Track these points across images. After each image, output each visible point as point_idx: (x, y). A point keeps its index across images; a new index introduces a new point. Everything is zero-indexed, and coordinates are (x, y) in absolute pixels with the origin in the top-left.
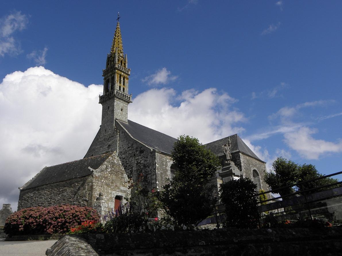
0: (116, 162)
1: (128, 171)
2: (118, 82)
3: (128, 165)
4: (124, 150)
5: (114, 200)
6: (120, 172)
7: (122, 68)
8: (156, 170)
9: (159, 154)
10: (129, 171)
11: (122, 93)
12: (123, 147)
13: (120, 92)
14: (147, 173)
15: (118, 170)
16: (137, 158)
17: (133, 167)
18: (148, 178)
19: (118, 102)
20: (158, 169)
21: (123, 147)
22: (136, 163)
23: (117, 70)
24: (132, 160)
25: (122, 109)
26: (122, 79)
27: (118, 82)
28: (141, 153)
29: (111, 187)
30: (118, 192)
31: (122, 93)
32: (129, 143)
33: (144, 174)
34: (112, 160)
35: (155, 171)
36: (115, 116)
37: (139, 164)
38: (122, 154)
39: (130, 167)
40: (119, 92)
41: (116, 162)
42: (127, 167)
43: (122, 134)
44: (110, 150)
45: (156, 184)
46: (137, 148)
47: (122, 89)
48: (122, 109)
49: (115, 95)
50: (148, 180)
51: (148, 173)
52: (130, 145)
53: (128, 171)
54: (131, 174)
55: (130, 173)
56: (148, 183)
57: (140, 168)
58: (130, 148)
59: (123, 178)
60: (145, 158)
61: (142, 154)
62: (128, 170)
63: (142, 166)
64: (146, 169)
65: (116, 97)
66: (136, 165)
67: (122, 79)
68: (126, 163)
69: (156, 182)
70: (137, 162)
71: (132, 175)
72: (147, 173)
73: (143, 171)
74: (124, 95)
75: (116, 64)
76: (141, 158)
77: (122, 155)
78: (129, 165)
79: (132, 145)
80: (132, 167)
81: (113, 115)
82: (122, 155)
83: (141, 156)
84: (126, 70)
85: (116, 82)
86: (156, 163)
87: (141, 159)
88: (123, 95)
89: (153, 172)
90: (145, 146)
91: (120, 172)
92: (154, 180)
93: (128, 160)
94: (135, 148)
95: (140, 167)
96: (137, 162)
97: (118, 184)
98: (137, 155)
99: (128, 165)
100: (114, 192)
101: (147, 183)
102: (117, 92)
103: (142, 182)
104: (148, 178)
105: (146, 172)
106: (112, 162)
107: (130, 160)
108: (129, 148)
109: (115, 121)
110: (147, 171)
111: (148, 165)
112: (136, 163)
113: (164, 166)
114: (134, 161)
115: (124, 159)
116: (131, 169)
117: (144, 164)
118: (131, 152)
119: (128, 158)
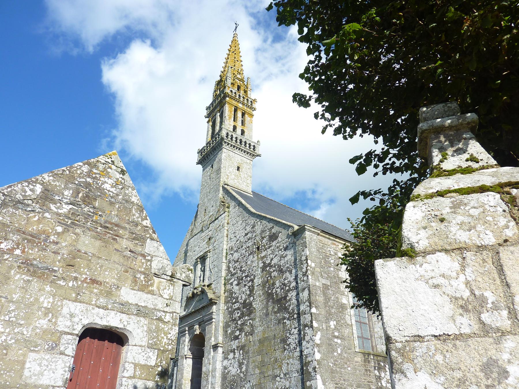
0: (113, 190)
1: (244, 289)
2: (230, 118)
3: (244, 275)
4: (238, 242)
5: (70, 346)
6: (125, 228)
7: (239, 95)
8: (308, 276)
9: (315, 237)
10: (247, 287)
11: (239, 138)
12: (235, 236)
13: (233, 134)
14: (287, 288)
15: (115, 220)
16: (262, 255)
17: (254, 278)
18: (289, 300)
19: (231, 154)
20: (313, 273)
21: (235, 236)
22: (261, 268)
23: (228, 97)
24: (252, 262)
25: (238, 168)
26: (239, 114)
27: (230, 118)
28: (273, 242)
29: (62, 283)
30: (105, 308)
31: (239, 138)
32: (247, 224)
33: (279, 290)
34: (89, 176)
35: (305, 278)
36: (223, 179)
37: (268, 269)
38: (232, 252)
39: (249, 279)
40: (232, 135)
41: (113, 190)
42: (242, 279)
43: (234, 210)
44: (211, 247)
45: (311, 314)
46: (263, 231)
47: (239, 131)
48: (238, 168)
49: (222, 139)
50: (290, 306)
51: (289, 286)
52: (249, 229)
53: (244, 289)
54: (250, 296)
55: (248, 293)
56: (289, 313)
57: (271, 277)
58: (249, 235)
59: (144, 256)
60: (281, 250)
61: (274, 243)
62: (245, 285)
63: (274, 271)
64: (284, 277)
65: (225, 142)
66: (262, 272)
67: (239, 114)
68: (241, 271)
69: (311, 308)
70: (264, 263)
71: (252, 298)
72: (287, 288)
73: (278, 284)
74: (244, 140)
75: (227, 87)
76: (273, 253)
77: (232, 254)
78: (246, 274)
79: (253, 228)
80: (252, 277)
81: (219, 178)
82: (232, 254)
83: (272, 248)
84: (247, 100)
85: (227, 118)
86: (307, 257)
87: (271, 256)
88: (241, 140)
89: (302, 283)
90: (279, 222)
91: (125, 228)
92: (305, 303)
93: (243, 264)
94: (258, 232)
95: (270, 273)
96: (264, 263)
97: (109, 277)
98: (264, 246)
99: (244, 275)
100: (75, 308)
101: (287, 316)
102: (227, 134)
103: (275, 313)
104: (289, 300)
105: (284, 284)
106: (87, 185)
107: (249, 263)
108: (246, 234)
109: (223, 187)
110: (286, 282)
111: (287, 265)
112: (261, 268)
113: (330, 267)
114: (258, 263)
115: (237, 261)
116: (250, 283)
117: (279, 266)
118: (250, 244)
119: (245, 259)
